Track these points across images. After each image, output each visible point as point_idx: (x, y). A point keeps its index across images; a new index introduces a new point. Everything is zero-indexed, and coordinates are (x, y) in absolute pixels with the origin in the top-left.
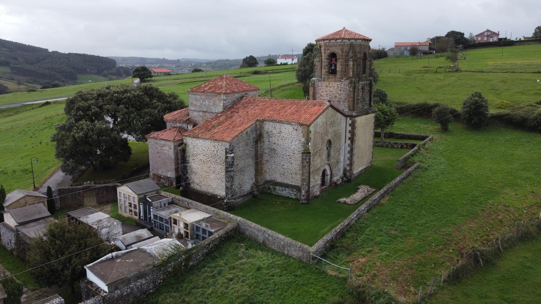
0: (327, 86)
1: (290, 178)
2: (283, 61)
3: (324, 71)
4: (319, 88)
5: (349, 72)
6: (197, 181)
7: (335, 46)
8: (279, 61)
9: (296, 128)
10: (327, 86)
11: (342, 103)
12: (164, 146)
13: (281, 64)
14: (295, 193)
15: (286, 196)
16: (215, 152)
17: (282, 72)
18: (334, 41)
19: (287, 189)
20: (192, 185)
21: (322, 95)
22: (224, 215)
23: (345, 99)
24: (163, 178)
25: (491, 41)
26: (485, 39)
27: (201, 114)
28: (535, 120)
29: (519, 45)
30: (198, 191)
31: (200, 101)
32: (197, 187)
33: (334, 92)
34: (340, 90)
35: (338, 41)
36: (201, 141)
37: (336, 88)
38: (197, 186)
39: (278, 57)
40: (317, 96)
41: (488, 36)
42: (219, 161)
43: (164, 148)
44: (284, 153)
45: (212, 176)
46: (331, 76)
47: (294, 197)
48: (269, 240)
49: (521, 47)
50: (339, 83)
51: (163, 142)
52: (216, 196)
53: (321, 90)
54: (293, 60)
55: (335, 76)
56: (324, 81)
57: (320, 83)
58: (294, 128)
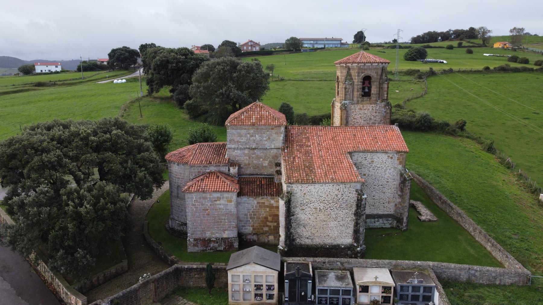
1: (381, 207)
2: (45, 69)
3: (356, 94)
4: (352, 111)
5: (384, 94)
6: (305, 234)
7: (371, 69)
8: (38, 69)
9: (391, 156)
11: (377, 125)
12: (219, 199)
13: (41, 74)
14: (390, 222)
15: (379, 227)
16: (339, 196)
17: (84, 82)
18: (370, 64)
19: (380, 220)
20: (298, 240)
21: (356, 117)
22: (407, 264)
23: (381, 121)
24: (214, 241)
25: (254, 50)
26: (250, 48)
27: (246, 152)
28: (418, 122)
29: (277, 54)
30: (308, 246)
31: (246, 136)
32: (308, 242)
33: (369, 114)
34: (376, 112)
35: (374, 64)
36: (317, 186)
37: (371, 110)
38: (306, 240)
39: (37, 62)
40: (350, 119)
41: (251, 46)
42: (344, 205)
43: (218, 202)
44: (376, 183)
45: (332, 224)
46: (365, 98)
47: (389, 226)
48: (475, 276)
49: (278, 56)
50: (374, 106)
51: (216, 195)
53: (355, 113)
54: (57, 67)
55: (370, 99)
57: (353, 107)
58: (389, 157)
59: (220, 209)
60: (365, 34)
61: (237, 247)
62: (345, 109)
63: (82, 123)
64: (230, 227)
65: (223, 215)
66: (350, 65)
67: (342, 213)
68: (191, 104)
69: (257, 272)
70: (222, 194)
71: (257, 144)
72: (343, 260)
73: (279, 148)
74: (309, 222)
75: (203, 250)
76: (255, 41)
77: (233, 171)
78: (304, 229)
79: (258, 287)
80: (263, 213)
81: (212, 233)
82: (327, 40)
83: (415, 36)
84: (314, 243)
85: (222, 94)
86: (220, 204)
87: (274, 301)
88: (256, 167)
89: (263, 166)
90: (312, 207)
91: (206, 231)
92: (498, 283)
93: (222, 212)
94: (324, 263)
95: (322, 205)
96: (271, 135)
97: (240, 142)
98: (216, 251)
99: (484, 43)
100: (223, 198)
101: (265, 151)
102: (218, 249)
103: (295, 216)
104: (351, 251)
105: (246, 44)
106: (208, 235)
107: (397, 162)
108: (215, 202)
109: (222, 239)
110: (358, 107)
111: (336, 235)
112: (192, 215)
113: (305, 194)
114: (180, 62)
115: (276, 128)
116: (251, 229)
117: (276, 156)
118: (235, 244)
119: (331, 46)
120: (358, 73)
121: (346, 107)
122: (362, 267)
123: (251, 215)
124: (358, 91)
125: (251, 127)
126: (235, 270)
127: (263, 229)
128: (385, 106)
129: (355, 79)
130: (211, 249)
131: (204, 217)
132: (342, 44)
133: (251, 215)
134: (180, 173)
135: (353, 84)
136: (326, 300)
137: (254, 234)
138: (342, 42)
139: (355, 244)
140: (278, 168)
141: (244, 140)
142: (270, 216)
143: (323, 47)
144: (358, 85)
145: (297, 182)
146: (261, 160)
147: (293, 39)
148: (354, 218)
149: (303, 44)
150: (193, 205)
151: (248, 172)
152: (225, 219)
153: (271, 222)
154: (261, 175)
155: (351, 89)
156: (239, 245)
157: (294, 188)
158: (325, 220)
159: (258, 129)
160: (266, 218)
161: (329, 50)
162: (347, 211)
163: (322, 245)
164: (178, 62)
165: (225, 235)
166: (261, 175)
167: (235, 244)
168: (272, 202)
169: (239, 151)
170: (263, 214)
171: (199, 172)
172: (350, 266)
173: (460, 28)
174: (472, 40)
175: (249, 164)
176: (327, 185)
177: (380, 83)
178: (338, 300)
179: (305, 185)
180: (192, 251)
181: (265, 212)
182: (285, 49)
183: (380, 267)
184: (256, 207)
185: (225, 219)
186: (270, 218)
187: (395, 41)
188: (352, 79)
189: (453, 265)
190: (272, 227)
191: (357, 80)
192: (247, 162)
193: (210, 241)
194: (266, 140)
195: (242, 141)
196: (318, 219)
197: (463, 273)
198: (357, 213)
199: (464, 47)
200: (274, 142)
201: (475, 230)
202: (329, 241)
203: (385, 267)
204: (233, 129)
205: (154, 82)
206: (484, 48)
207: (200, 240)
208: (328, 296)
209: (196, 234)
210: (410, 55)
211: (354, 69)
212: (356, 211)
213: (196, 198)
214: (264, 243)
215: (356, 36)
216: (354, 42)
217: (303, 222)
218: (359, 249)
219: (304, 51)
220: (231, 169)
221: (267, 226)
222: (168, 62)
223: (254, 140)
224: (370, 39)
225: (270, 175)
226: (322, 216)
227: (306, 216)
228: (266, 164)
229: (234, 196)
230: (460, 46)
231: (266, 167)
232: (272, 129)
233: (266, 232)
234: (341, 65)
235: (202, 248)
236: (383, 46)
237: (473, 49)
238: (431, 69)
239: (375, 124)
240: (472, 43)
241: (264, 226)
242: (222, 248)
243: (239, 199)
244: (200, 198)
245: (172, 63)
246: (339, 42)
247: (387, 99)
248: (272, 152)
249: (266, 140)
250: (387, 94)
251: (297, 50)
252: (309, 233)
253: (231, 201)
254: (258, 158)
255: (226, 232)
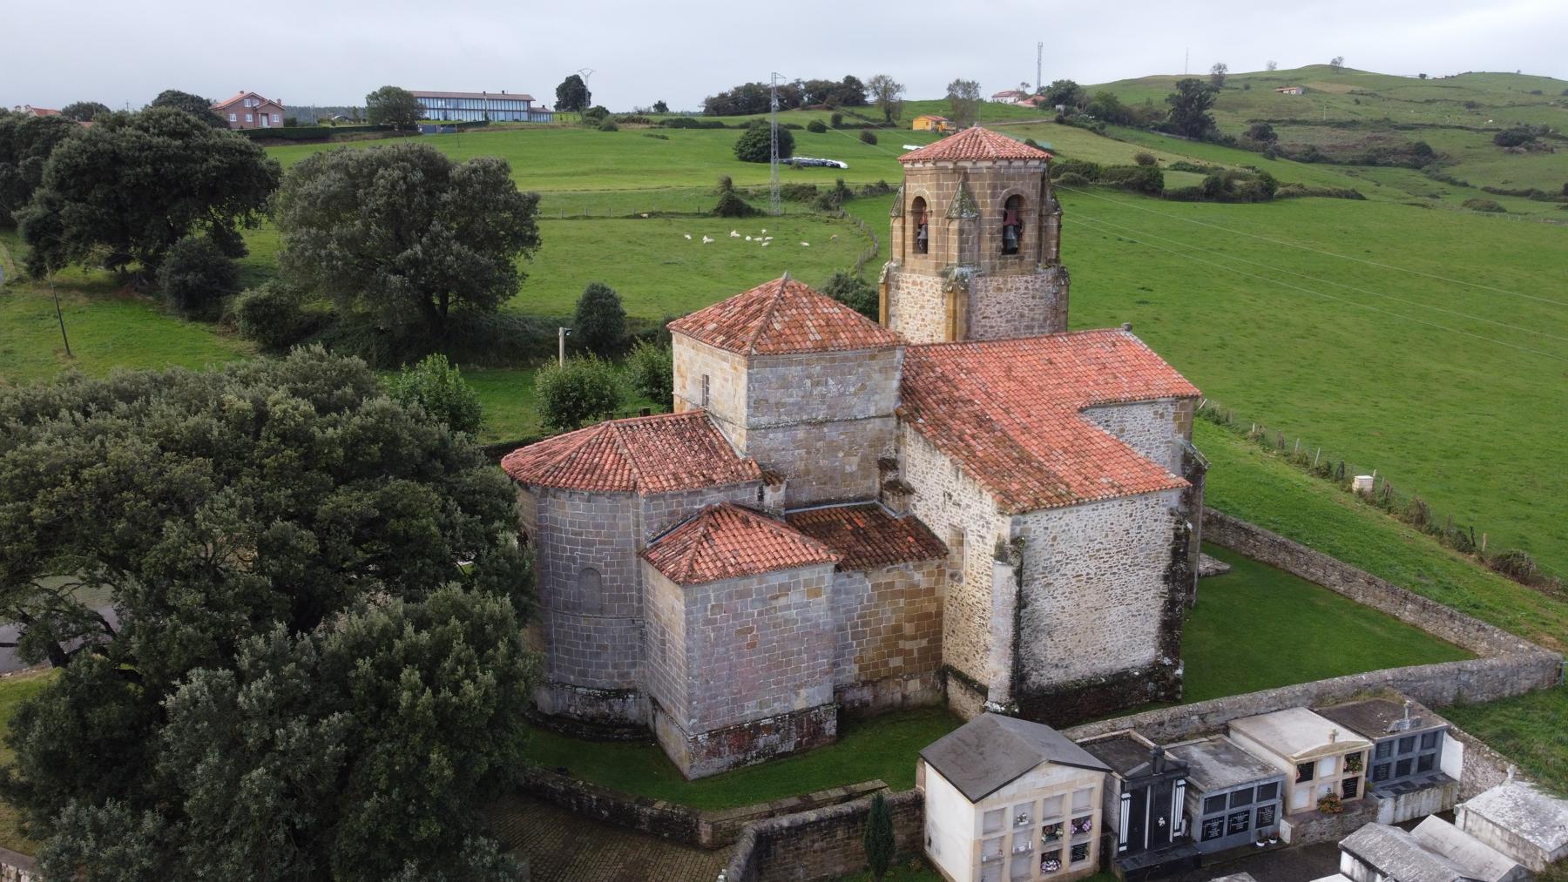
0: (999, 289)
4: (980, 295)
7: (1022, 177)
10: (999, 289)
12: (784, 589)
18: (1021, 163)
24: (768, 728)
25: (265, 125)
26: (249, 118)
30: (1057, 687)
35: (1031, 163)
36: (1084, 510)
41: (254, 110)
42: (1142, 555)
43: (782, 601)
45: (1115, 613)
46: (1010, 259)
50: (1029, 278)
52: (1126, 672)
55: (1022, 258)
56: (993, 274)
58: (1156, 413)
59: (786, 621)
60: (590, 85)
61: (833, 731)
62: (966, 291)
63: (725, 359)
64: (812, 675)
65: (795, 639)
66: (968, 165)
67: (1135, 581)
68: (266, 302)
69: (1050, 788)
70: (794, 572)
71: (830, 407)
72: (1200, 706)
73: (888, 416)
74: (1062, 617)
75: (737, 764)
76: (268, 97)
77: (773, 497)
78: (1049, 643)
79: (1051, 833)
80: (889, 615)
81: (761, 705)
82: (493, 98)
83: (715, 95)
84: (1072, 678)
85: (413, 262)
86: (788, 607)
87: (1089, 863)
88: (828, 478)
89: (844, 474)
90: (1069, 573)
91: (746, 698)
92: (1507, 693)
93: (791, 630)
94: (1161, 724)
95: (1092, 563)
96: (869, 377)
97: (784, 405)
98: (775, 757)
99: (889, 119)
100: (797, 584)
101: (851, 428)
102: (780, 751)
103: (1029, 608)
104: (1156, 682)
105: (236, 105)
106: (750, 711)
107: (1172, 426)
108: (774, 603)
109: (792, 715)
110: (994, 282)
111: (1120, 644)
112: (704, 656)
113: (1054, 539)
114: (169, 159)
115: (881, 355)
116: (855, 668)
117: (879, 439)
118: (827, 726)
119: (502, 116)
120: (994, 187)
121: (966, 286)
122: (1253, 715)
123: (855, 626)
124: (992, 239)
125: (815, 356)
126: (995, 795)
127: (887, 663)
128: (1056, 278)
129: (984, 204)
130: (758, 757)
131: (740, 656)
132: (532, 112)
133: (855, 626)
134: (596, 526)
135: (977, 220)
136: (1221, 826)
137: (865, 684)
138: (533, 105)
139: (1167, 661)
140: (890, 476)
141: (795, 396)
142: (910, 620)
143: (479, 118)
144: (991, 222)
145: (1037, 505)
146: (841, 454)
147: (388, 92)
148: (1163, 588)
149: (423, 108)
150: (708, 622)
151: (804, 497)
152: (800, 653)
153: (914, 638)
154: (840, 501)
155: (975, 234)
156: (840, 728)
157: (1029, 525)
158: (1098, 605)
159: (833, 360)
160: (897, 629)
161: (501, 128)
162: (1147, 571)
163: (1090, 681)
164: (161, 156)
165: (799, 704)
166: (840, 501)
167: (827, 726)
168: (918, 577)
169: (780, 435)
170: (889, 619)
171: (672, 514)
172: (1221, 720)
173: (821, 76)
174: (858, 110)
175: (808, 472)
176: (1107, 505)
177: (1041, 215)
178: (1247, 818)
179: (1056, 514)
180: (704, 773)
181: (894, 611)
182: (367, 124)
183: (1287, 708)
184: (870, 599)
185: (800, 653)
186: (908, 629)
187: (661, 107)
188: (974, 204)
189: (1428, 669)
190: (916, 655)
191: (990, 208)
192: (800, 466)
193: (756, 728)
194: (855, 394)
195: (791, 400)
196: (1083, 606)
197: (1447, 684)
198: (1174, 573)
199: (848, 127)
200: (877, 397)
201: (1346, 579)
202: (1105, 665)
203: (1296, 706)
204: (766, 365)
205: (60, 231)
206: (891, 130)
207: (729, 732)
208: (1228, 811)
209: (716, 716)
210: (754, 145)
211: (979, 176)
212: (1170, 567)
213: (717, 598)
214: (891, 705)
215: (562, 91)
216: (558, 107)
217: (1047, 621)
218: (1180, 672)
219: (426, 130)
220: (768, 491)
221: (901, 652)
222: (116, 159)
223: (823, 396)
224: (605, 95)
225: (862, 499)
226: (1092, 598)
227: (1054, 602)
228: (852, 465)
229: (827, 575)
230: (837, 122)
231: (851, 474)
232: (873, 357)
233: (896, 673)
234: (940, 164)
235: (732, 758)
236: (648, 122)
237: (874, 132)
238: (840, 183)
239: (1032, 328)
240: (859, 116)
241: (890, 655)
242: (790, 746)
243: (843, 578)
244: (730, 596)
245: (136, 162)
246: (523, 107)
247: (1057, 260)
248: (869, 427)
249: (855, 394)
250: (1058, 245)
251: (407, 127)
252: (1061, 650)
253: (816, 593)
254: (833, 448)
255: (803, 692)
